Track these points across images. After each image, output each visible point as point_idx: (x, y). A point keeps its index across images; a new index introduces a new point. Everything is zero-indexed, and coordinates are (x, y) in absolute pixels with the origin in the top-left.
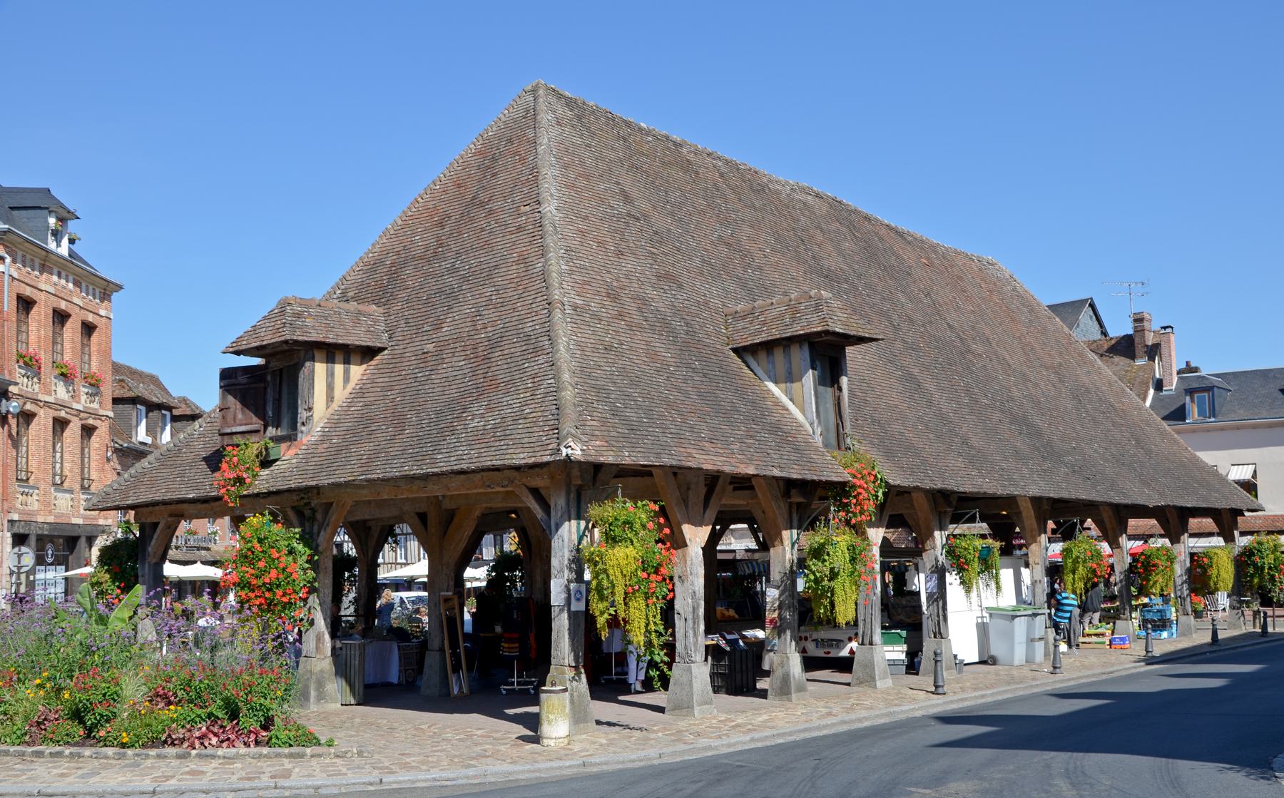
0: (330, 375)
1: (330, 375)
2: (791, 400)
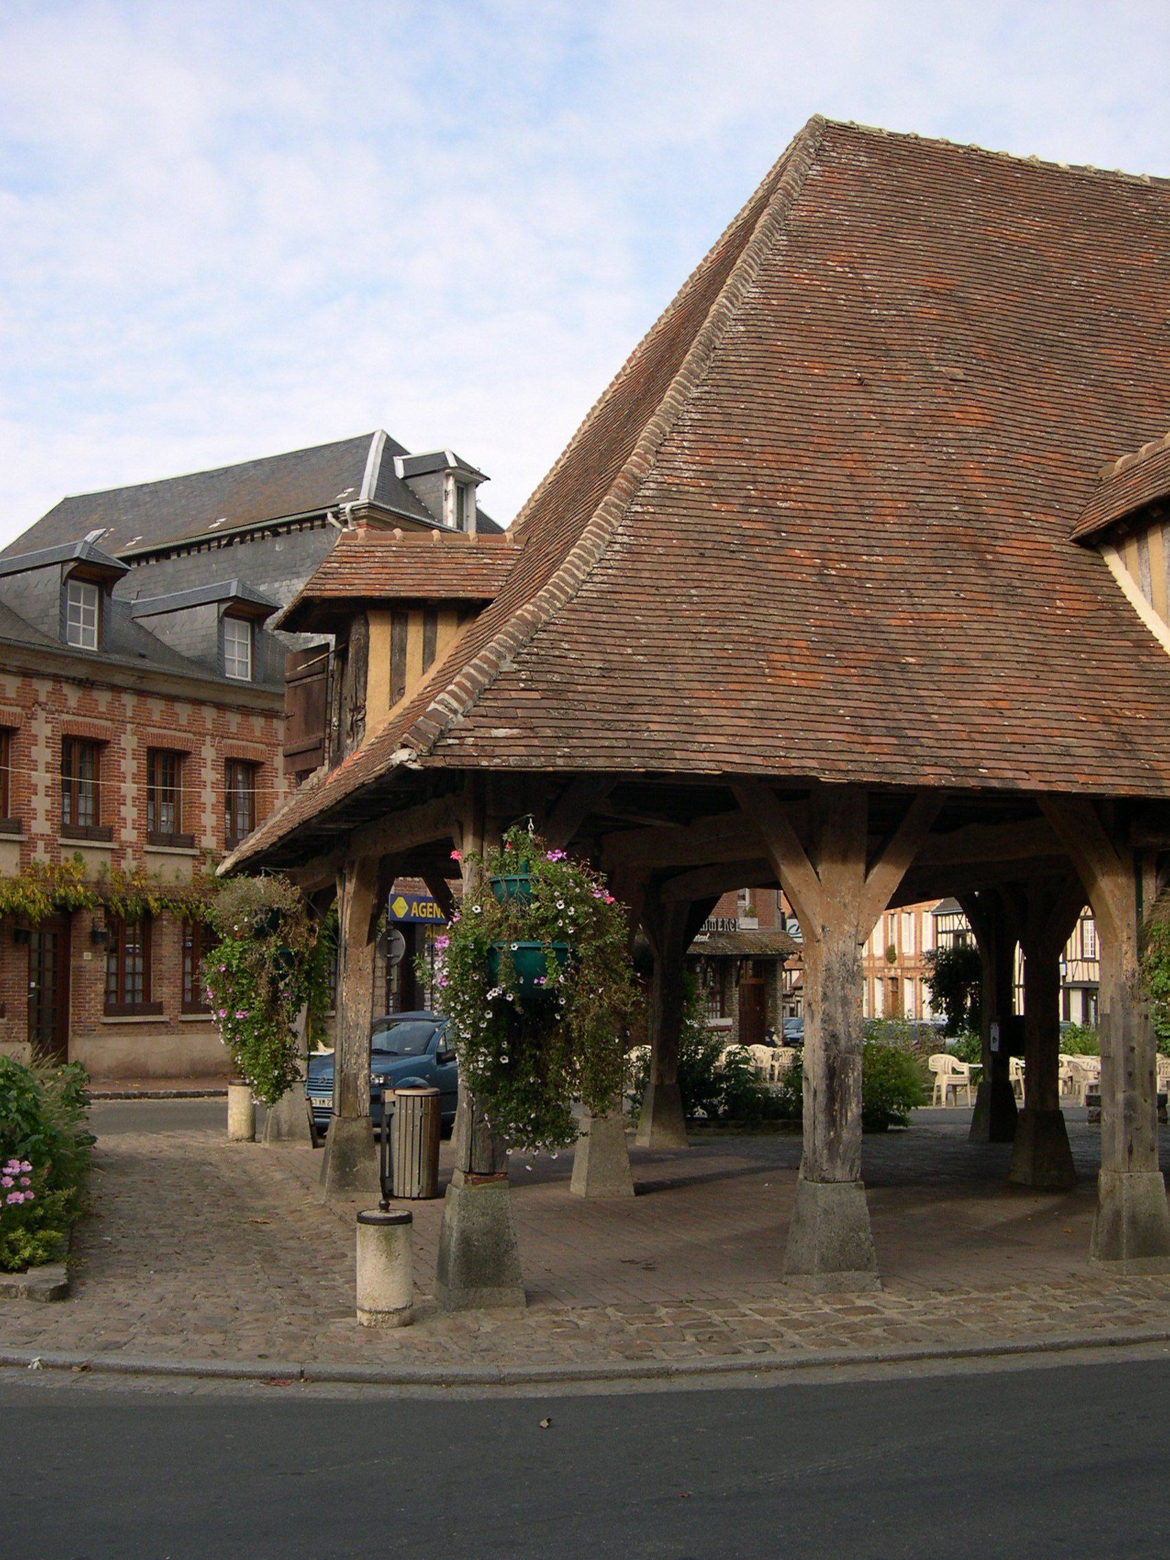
0: (398, 650)
1: (398, 650)
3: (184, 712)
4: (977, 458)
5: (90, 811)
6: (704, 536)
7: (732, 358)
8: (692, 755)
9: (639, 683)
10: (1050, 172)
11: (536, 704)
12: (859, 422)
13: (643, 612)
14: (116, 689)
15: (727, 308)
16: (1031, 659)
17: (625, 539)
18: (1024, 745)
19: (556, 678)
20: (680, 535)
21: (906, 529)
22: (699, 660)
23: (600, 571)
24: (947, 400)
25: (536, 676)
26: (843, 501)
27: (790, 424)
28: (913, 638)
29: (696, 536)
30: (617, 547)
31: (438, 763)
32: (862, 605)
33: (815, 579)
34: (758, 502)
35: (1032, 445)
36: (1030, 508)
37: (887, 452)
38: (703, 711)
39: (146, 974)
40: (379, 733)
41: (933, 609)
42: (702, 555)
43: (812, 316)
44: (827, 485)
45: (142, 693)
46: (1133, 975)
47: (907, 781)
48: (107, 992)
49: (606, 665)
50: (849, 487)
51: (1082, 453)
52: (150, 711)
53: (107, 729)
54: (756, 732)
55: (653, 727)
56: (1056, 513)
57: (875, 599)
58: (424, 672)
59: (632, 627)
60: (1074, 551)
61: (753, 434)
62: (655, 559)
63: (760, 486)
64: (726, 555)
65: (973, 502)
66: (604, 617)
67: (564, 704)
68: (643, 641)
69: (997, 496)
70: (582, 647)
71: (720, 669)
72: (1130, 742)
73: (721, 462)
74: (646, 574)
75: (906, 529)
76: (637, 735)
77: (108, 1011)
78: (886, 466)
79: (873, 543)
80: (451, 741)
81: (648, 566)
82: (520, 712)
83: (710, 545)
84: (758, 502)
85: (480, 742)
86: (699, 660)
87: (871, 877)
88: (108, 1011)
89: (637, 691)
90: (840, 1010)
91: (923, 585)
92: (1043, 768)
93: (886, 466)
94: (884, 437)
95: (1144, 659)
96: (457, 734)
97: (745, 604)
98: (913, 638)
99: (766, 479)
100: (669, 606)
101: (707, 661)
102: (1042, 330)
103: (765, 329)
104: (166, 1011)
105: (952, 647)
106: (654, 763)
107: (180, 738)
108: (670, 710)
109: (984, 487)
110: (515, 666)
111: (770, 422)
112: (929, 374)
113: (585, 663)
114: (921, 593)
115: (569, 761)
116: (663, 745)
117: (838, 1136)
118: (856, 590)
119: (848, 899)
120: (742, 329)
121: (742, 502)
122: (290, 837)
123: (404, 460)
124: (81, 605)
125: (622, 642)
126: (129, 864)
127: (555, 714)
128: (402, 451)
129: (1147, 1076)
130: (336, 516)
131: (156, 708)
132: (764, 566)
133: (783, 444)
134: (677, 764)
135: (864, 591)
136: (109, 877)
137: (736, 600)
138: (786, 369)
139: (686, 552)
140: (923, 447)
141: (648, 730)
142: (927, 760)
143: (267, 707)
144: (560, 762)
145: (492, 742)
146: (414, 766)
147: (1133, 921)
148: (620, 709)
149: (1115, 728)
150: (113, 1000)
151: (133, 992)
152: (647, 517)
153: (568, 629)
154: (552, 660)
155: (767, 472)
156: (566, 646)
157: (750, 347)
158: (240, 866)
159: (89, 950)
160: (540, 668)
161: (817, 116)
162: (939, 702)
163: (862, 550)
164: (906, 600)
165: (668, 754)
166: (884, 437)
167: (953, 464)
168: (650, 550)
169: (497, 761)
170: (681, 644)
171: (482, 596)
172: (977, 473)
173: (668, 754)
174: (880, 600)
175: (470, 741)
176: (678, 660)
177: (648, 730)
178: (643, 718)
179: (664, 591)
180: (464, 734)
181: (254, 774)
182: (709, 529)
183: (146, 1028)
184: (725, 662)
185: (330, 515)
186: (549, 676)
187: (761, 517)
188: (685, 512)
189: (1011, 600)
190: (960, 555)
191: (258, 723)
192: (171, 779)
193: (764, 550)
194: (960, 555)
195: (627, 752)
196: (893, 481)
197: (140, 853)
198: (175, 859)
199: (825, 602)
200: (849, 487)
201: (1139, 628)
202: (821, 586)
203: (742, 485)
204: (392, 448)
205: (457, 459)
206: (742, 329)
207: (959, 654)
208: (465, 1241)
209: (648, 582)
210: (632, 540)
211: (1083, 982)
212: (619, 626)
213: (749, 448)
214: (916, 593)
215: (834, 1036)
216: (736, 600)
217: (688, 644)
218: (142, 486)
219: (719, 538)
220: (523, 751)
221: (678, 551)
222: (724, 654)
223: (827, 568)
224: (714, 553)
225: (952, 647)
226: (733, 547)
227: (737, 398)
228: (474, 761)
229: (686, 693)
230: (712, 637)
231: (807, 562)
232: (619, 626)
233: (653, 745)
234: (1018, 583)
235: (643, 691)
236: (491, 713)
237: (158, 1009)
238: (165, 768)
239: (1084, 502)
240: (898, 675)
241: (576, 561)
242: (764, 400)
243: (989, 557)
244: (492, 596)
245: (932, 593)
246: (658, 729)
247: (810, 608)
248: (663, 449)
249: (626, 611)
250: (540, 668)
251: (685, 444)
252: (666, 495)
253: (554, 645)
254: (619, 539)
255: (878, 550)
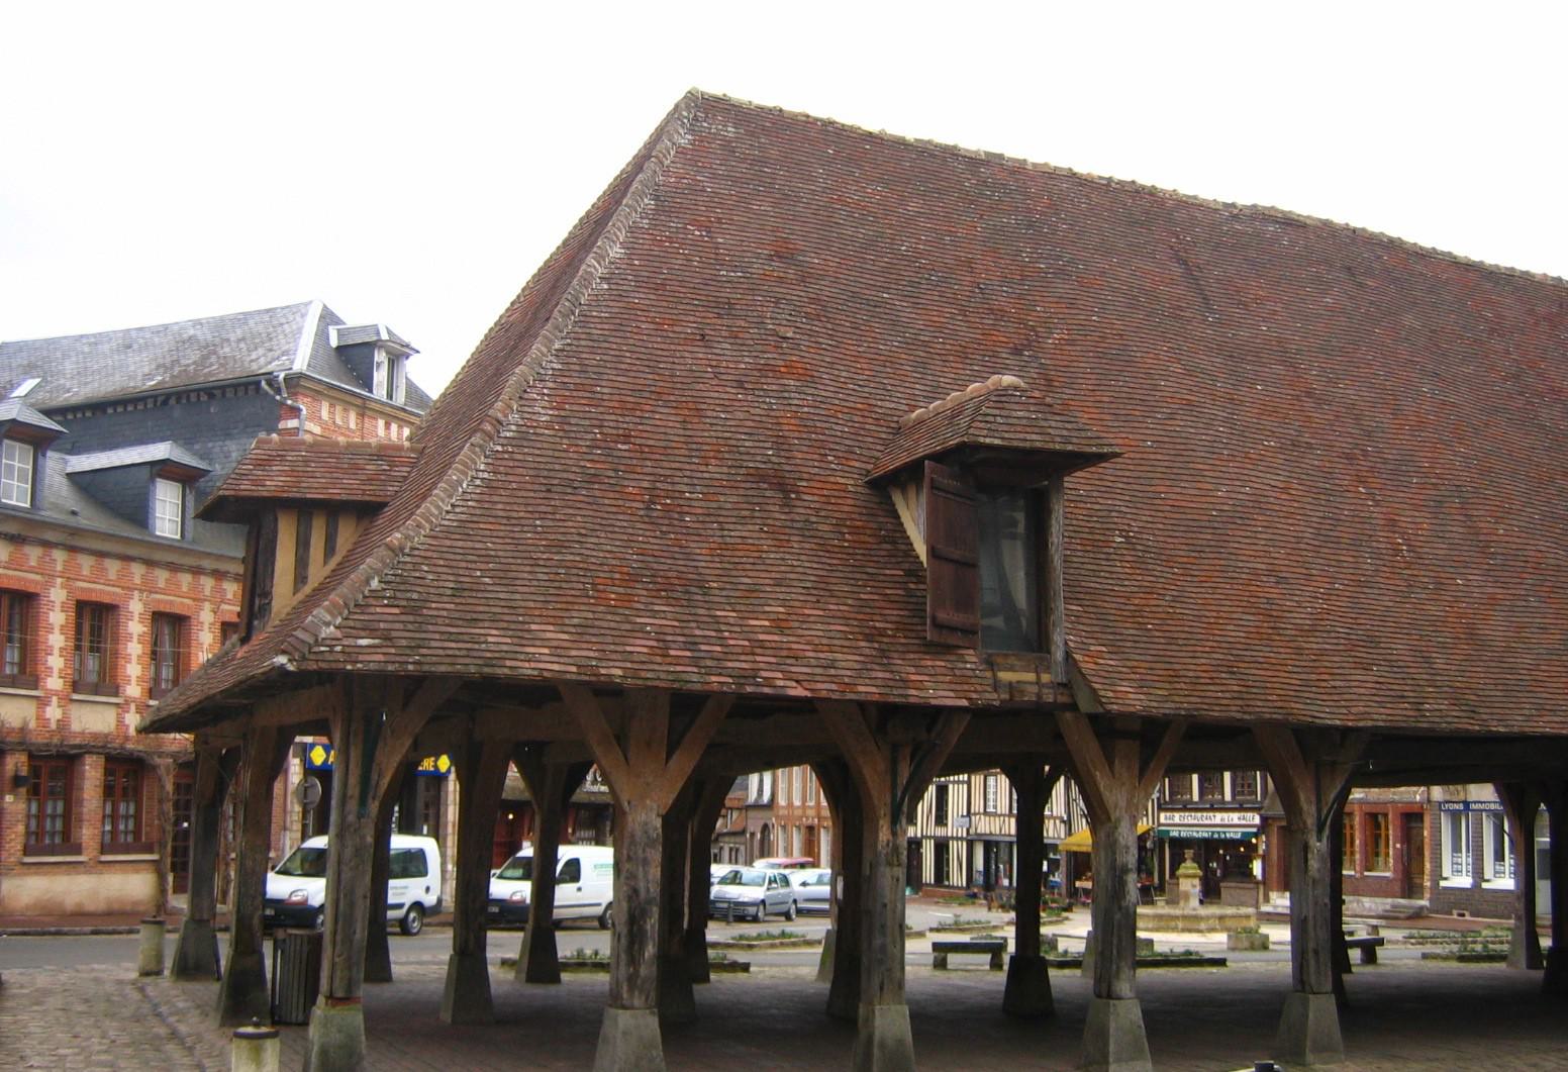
0: (303, 545)
3: (113, 567)
4: (794, 408)
5: (16, 660)
6: (552, 474)
7: (595, 314)
8: (520, 664)
9: (483, 601)
10: (900, 144)
11: (396, 618)
12: (698, 374)
13: (494, 540)
14: (47, 545)
15: (595, 267)
16: (815, 585)
17: (486, 475)
18: (796, 658)
19: (415, 596)
20: (531, 472)
21: (725, 470)
22: (535, 583)
23: (461, 503)
24: (775, 356)
25: (399, 594)
26: (674, 445)
27: (638, 375)
28: (719, 565)
29: (546, 473)
30: (478, 482)
32: (679, 537)
33: (642, 513)
34: (603, 445)
35: (844, 397)
36: (834, 453)
37: (717, 402)
38: (533, 627)
39: (67, 816)
40: (283, 616)
41: (739, 541)
42: (549, 491)
43: (669, 277)
44: (662, 430)
45: (73, 549)
46: (888, 845)
47: (698, 687)
48: (28, 833)
49: (459, 586)
50: (681, 432)
51: (888, 404)
52: (80, 566)
53: (37, 583)
54: (575, 645)
55: (490, 639)
56: (856, 457)
57: (691, 531)
58: (325, 563)
59: (483, 553)
61: (604, 383)
62: (508, 493)
63: (605, 431)
64: (569, 490)
65: (786, 447)
66: (460, 544)
67: (419, 619)
68: (491, 565)
69: (807, 443)
70: (440, 570)
71: (552, 591)
72: (887, 658)
73: (575, 408)
74: (500, 506)
75: (725, 470)
76: (476, 646)
77: (27, 851)
78: (715, 414)
79: (696, 481)
80: (323, 649)
81: (504, 499)
82: (382, 625)
83: (556, 482)
84: (603, 445)
85: (347, 650)
86: (535, 583)
87: (672, 763)
88: (27, 851)
89: (481, 609)
90: (641, 869)
91: (734, 520)
92: (811, 678)
93: (715, 414)
94: (716, 388)
95: (912, 586)
96: (328, 642)
97: (579, 534)
98: (719, 565)
99: (611, 424)
100: (517, 535)
101: (542, 583)
102: (868, 292)
103: (625, 288)
104: (85, 852)
105: (750, 574)
106: (486, 670)
107: (109, 593)
108: (505, 625)
109: (796, 435)
110: (383, 586)
111: (620, 372)
112: (762, 331)
113: (441, 584)
114: (731, 527)
115: (418, 667)
116: (497, 655)
117: (637, 972)
118: (676, 522)
119: (650, 779)
120: (606, 286)
121: (588, 443)
122: (199, 706)
123: (338, 330)
124: (17, 464)
125: (473, 566)
126: (53, 712)
127: (410, 627)
128: (336, 321)
129: (897, 927)
130: (269, 383)
131: (86, 563)
132: (601, 501)
133: (630, 393)
134: (506, 671)
135: (682, 524)
136: (32, 725)
137: (573, 530)
138: (639, 324)
139: (536, 487)
140: (749, 398)
141: (486, 642)
142: (714, 671)
143: (194, 564)
144: (411, 667)
145: (357, 650)
147: (888, 800)
148: (465, 624)
149: (876, 645)
150: (33, 841)
151: (53, 834)
152: (506, 456)
153: (429, 554)
154: (412, 580)
155: (613, 417)
156: (426, 568)
157: (611, 304)
158: (156, 726)
159: (10, 793)
160: (402, 587)
161: (694, 88)
162: (732, 621)
163: (685, 488)
164: (718, 533)
165: (500, 663)
166: (716, 388)
167: (773, 414)
168: (506, 485)
169: (359, 665)
170: (522, 568)
171: (379, 499)
172: (793, 421)
173: (500, 663)
174: (695, 532)
175: (339, 648)
176: (518, 582)
177: (486, 642)
178: (482, 631)
179: (513, 522)
180: (334, 643)
181: (180, 626)
182: (557, 467)
183: (64, 867)
184: (557, 584)
185: (263, 383)
186: (409, 595)
187: (603, 458)
188: (538, 452)
189: (807, 533)
190: (768, 493)
191: (186, 579)
192: (97, 634)
193: (603, 487)
194: (768, 493)
195: (467, 661)
196: (719, 428)
197: (66, 701)
198: (100, 708)
199: (648, 533)
200: (681, 432)
201: (912, 559)
202: (646, 520)
203: (589, 429)
204: (328, 318)
205: (389, 332)
206: (606, 286)
207: (755, 581)
208: (324, 1052)
209: (501, 513)
210: (491, 476)
211: (985, 834)
212: (471, 552)
213: (599, 396)
214: (727, 526)
215: (635, 891)
216: (573, 530)
217: (528, 569)
218: (82, 336)
219: (565, 475)
220: (381, 658)
221: (529, 487)
222: (558, 578)
223: (654, 503)
224: (559, 489)
225: (750, 574)
226: (576, 484)
227: (595, 350)
228: (341, 666)
229: (521, 611)
230: (548, 563)
231: (638, 498)
232: (471, 552)
233: (489, 655)
234: (814, 519)
235: (486, 609)
236: (358, 624)
237: (77, 849)
238: (93, 619)
239: (882, 448)
240: (699, 598)
241: (442, 494)
242: (617, 353)
243: (793, 496)
244: (388, 499)
245: (739, 527)
246: (495, 639)
247: (635, 538)
248: (526, 396)
249: (479, 538)
250: (402, 587)
251: (545, 391)
252: (522, 436)
253: (416, 566)
254: (481, 475)
255: (698, 488)
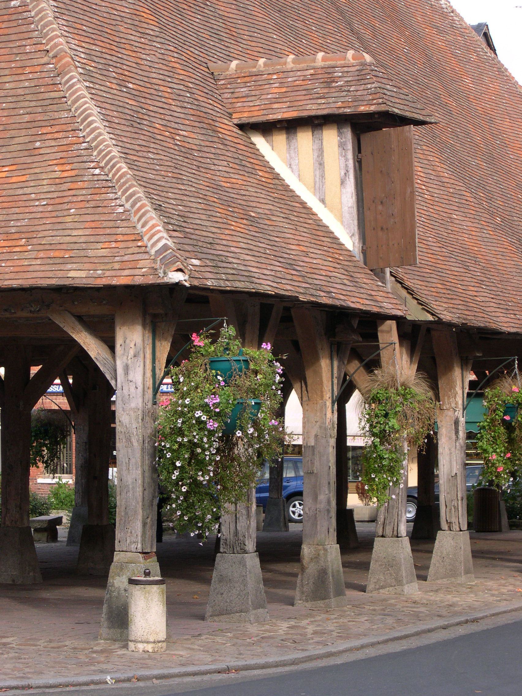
2: (323, 201)
31: (196, 283)
60: (235, 130)
146: (187, 284)
